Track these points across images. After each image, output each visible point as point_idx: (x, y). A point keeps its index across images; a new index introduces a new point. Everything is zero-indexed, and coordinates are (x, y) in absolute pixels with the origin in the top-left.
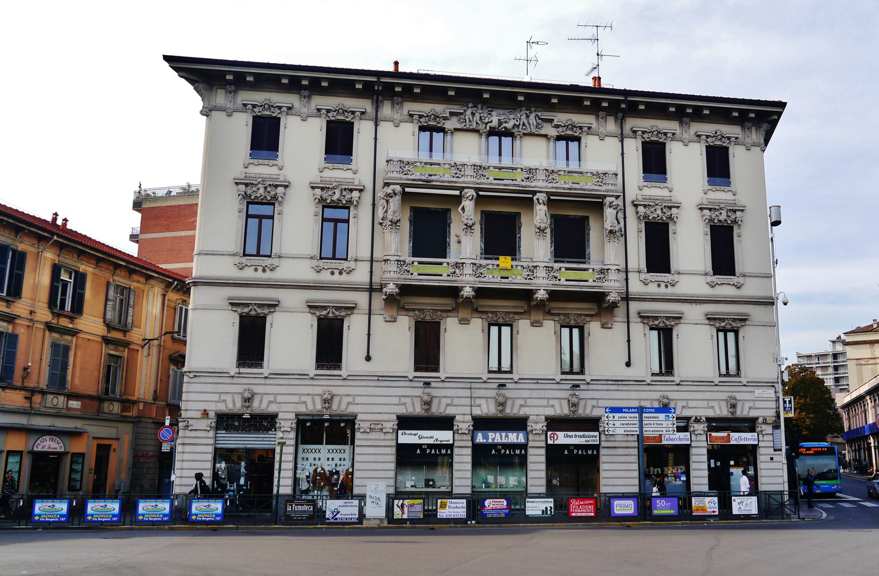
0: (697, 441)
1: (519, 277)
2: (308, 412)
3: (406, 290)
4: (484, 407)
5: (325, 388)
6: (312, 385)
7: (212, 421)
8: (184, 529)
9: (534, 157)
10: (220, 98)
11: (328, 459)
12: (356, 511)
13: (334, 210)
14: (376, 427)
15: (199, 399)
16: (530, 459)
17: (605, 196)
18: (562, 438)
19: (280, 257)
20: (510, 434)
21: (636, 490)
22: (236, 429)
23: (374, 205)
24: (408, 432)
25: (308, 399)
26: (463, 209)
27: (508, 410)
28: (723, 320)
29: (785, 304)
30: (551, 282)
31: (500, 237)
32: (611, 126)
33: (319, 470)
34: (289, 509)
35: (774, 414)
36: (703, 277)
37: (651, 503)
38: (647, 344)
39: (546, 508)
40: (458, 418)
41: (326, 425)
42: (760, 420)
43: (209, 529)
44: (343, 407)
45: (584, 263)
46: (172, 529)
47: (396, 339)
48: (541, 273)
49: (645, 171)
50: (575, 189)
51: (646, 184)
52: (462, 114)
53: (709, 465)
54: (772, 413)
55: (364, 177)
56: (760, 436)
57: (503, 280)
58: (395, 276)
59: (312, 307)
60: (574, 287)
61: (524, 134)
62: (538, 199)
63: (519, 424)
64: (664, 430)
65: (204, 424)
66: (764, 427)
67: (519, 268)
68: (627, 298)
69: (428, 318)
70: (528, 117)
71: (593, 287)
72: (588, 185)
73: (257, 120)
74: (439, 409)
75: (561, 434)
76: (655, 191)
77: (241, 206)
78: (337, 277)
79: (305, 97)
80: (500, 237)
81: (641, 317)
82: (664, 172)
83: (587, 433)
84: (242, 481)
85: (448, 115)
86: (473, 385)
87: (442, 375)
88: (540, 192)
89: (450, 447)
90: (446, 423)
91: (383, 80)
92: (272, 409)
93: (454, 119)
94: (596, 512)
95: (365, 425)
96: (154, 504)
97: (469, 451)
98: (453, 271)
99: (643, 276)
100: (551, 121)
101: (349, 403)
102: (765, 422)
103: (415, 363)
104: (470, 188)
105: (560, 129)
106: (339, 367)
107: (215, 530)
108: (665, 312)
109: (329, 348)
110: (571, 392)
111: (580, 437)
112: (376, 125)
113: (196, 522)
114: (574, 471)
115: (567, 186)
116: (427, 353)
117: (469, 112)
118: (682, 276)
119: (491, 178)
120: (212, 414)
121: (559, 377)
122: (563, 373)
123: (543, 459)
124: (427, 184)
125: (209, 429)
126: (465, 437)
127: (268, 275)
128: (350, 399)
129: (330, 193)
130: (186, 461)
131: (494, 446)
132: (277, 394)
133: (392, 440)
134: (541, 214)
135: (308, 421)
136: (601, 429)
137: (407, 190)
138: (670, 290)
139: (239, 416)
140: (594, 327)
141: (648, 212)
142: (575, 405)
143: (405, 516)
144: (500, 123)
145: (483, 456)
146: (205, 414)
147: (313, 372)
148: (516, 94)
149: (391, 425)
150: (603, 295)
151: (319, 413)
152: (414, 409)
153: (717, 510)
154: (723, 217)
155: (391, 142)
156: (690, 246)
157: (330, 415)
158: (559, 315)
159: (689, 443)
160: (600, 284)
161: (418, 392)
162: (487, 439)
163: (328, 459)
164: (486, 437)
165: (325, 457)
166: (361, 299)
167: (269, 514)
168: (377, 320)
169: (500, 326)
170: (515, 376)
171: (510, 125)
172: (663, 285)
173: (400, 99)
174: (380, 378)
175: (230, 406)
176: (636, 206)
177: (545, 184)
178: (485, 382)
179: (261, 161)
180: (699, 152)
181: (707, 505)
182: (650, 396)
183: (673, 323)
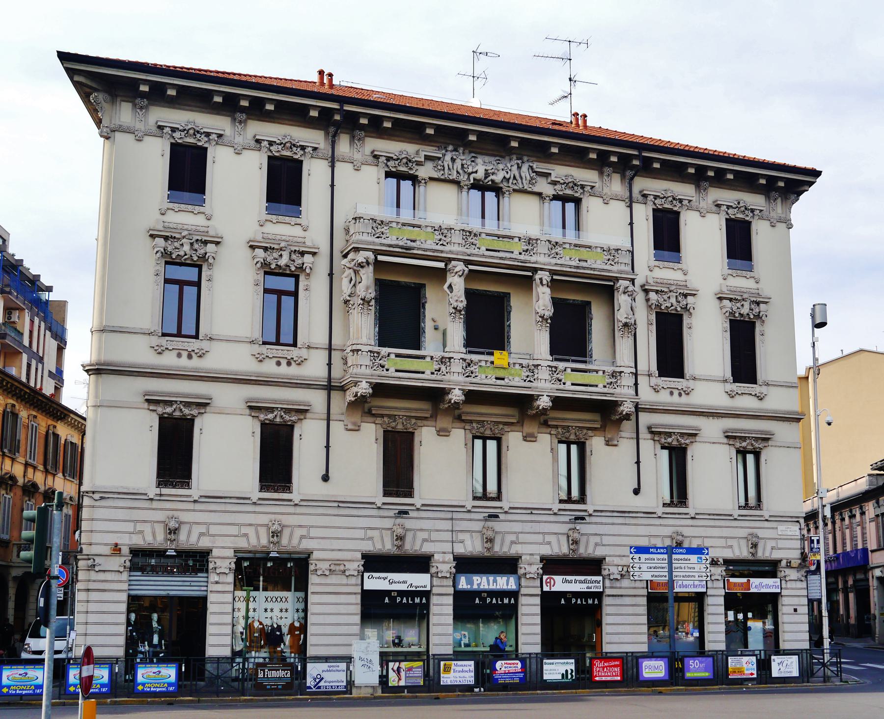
0: (713, 588)
1: (517, 379)
2: (250, 548)
3: (381, 390)
4: (377, 540)
5: (273, 517)
6: (255, 512)
7: (125, 559)
8: (131, 703)
9: (526, 220)
10: (125, 113)
11: (266, 610)
13: (281, 281)
14: (337, 568)
15: (106, 531)
16: (434, 609)
17: (617, 279)
18: (560, 584)
20: (499, 579)
22: (154, 570)
23: (331, 275)
24: (375, 575)
25: (251, 531)
26: (450, 287)
27: (497, 548)
28: (743, 439)
29: (829, 424)
30: (555, 386)
31: (486, 326)
32: (616, 185)
33: (256, 624)
34: (261, 675)
35: (799, 556)
36: (721, 385)
37: (683, 664)
38: (658, 464)
39: (567, 671)
40: (436, 557)
41: (269, 565)
42: (784, 563)
43: (431, 697)
44: (295, 542)
45: (585, 362)
46: (115, 703)
47: (360, 453)
48: (543, 374)
49: (269, 200)
50: (584, 268)
51: (657, 263)
52: (439, 158)
53: (128, 620)
54: (796, 554)
55: (317, 237)
56: (783, 582)
57: (499, 382)
58: (369, 371)
59: (254, 408)
61: (514, 190)
62: (541, 279)
64: (696, 574)
65: (116, 563)
68: (637, 408)
69: (400, 427)
70: (519, 168)
71: (605, 394)
73: (176, 149)
74: (414, 546)
75: (558, 579)
76: (667, 274)
77: (158, 267)
78: (284, 369)
79: (240, 122)
80: (486, 326)
81: (652, 432)
82: (202, 191)
83: (589, 578)
85: (423, 159)
86: (455, 516)
87: (417, 501)
88: (542, 269)
89: (426, 594)
90: (421, 563)
91: (347, 108)
92: (204, 543)
93: (429, 165)
94: (622, 675)
95: (324, 566)
96: (22, 671)
97: (450, 600)
98: (437, 367)
100: (547, 175)
102: (789, 565)
104: (459, 260)
105: (558, 187)
106: (188, 485)
107: (170, 704)
108: (679, 427)
109: (276, 463)
110: (572, 526)
111: (581, 582)
112: (333, 167)
113: (144, 694)
114: (572, 624)
116: (398, 474)
117: (448, 157)
118: (698, 383)
119: (483, 248)
120: (125, 550)
121: (556, 506)
122: (475, 498)
123: (538, 610)
124: (407, 252)
125: (122, 569)
127: (195, 363)
128: (303, 532)
130: (93, 612)
131: (478, 593)
132: (707, 537)
133: (643, 588)
134: (543, 299)
135: (246, 559)
136: (605, 573)
137: (380, 258)
138: (684, 399)
139: (160, 553)
141: (661, 301)
142: (401, 538)
143: (402, 683)
144: (487, 174)
145: (468, 608)
146: (116, 549)
148: (508, 138)
149: (356, 565)
150: (615, 404)
151: (264, 549)
152: (384, 546)
153: (755, 672)
154: (745, 310)
155: (350, 189)
156: (707, 345)
157: (176, 551)
158: (556, 427)
159: (704, 590)
160: (612, 391)
161: (388, 523)
162: (472, 584)
163: (266, 610)
165: (274, 608)
166: (316, 399)
167: (202, 683)
168: (337, 427)
169: (484, 439)
170: (505, 504)
171: (498, 178)
172: (676, 392)
173: (244, 116)
174: (341, 503)
175: (149, 538)
176: (646, 291)
177: (547, 260)
178: (469, 511)
179: (183, 207)
180: (718, 227)
181: (745, 666)
182: (659, 533)
183: (687, 441)
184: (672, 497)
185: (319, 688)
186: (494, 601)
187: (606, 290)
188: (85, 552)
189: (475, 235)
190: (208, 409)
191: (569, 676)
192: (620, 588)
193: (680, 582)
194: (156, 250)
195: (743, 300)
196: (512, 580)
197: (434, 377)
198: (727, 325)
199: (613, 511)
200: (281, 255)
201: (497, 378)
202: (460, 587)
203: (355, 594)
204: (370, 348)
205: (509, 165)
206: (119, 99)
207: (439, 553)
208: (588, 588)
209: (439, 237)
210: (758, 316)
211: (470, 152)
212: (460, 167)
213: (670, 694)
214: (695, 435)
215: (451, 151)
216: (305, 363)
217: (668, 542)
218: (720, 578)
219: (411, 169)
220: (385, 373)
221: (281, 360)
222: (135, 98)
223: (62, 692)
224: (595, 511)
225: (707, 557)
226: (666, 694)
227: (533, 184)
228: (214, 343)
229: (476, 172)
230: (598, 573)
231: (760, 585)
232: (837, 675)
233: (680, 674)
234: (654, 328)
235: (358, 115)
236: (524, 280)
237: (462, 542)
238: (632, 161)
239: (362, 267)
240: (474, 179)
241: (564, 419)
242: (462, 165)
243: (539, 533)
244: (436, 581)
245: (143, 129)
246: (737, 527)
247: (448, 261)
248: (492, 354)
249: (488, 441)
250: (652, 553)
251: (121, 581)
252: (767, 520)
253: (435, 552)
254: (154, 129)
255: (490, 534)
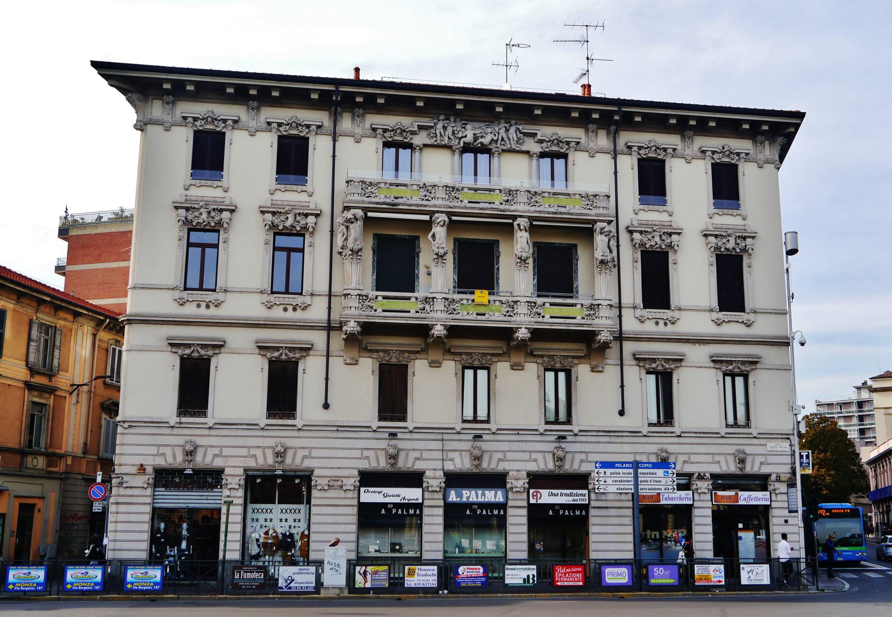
1: (497, 314)
2: (258, 467)
3: (369, 329)
5: (278, 440)
6: (263, 436)
7: (149, 477)
9: (515, 176)
10: (157, 110)
11: (281, 520)
12: (312, 578)
13: (287, 238)
14: (335, 484)
15: (133, 453)
17: (595, 221)
18: (546, 497)
19: (226, 291)
20: (487, 492)
21: (630, 555)
22: (177, 487)
24: (371, 489)
26: (434, 236)
27: (485, 465)
28: (730, 362)
29: (802, 344)
30: (534, 320)
31: (476, 267)
32: (602, 140)
34: (237, 577)
36: (707, 314)
37: (647, 571)
38: (643, 390)
39: (528, 576)
40: (428, 473)
42: (773, 477)
43: (393, 598)
45: (572, 297)
46: (104, 599)
47: (356, 385)
48: (522, 309)
50: (561, 213)
52: (432, 127)
54: (787, 469)
56: (773, 495)
57: (479, 317)
58: (357, 312)
59: (263, 348)
60: (560, 325)
62: (519, 225)
63: (498, 480)
66: (777, 485)
67: (497, 303)
68: (620, 337)
69: (394, 361)
70: (507, 130)
72: (576, 209)
74: (406, 463)
75: (545, 492)
76: (653, 215)
77: (181, 234)
80: (476, 267)
83: (575, 491)
84: (184, 545)
85: (416, 129)
86: (445, 437)
87: (410, 424)
88: (521, 216)
89: (419, 506)
90: (414, 479)
91: (342, 89)
92: (218, 463)
95: (323, 482)
96: (84, 571)
97: (441, 511)
98: (422, 306)
99: (639, 312)
100: (534, 135)
101: (304, 457)
102: (778, 480)
103: (379, 412)
105: (544, 145)
106: (204, 415)
107: (153, 600)
109: (282, 395)
111: (566, 495)
113: (132, 591)
114: (560, 535)
115: (552, 210)
116: (393, 400)
117: (440, 126)
118: (683, 313)
119: (466, 201)
120: (149, 470)
123: (525, 520)
124: (393, 208)
125: (146, 486)
126: (436, 496)
127: (213, 311)
129: (282, 218)
131: (469, 505)
132: (314, 448)
134: (522, 242)
135: (258, 476)
136: (591, 487)
137: (370, 214)
138: (670, 328)
139: (180, 472)
140: (582, 371)
141: (645, 240)
142: (561, 459)
143: (368, 585)
144: (476, 138)
145: (457, 518)
146: (142, 469)
147: (263, 421)
149: (352, 481)
151: (271, 468)
153: (723, 579)
154: (731, 245)
155: (351, 159)
156: (693, 278)
157: (283, 471)
160: (589, 322)
161: (383, 444)
162: (461, 497)
163: (281, 520)
164: (459, 495)
165: (278, 518)
166: (318, 338)
167: (214, 583)
168: (337, 363)
169: (475, 369)
171: (486, 140)
172: (661, 322)
173: (361, 111)
174: (340, 428)
175: (170, 460)
176: (631, 232)
177: (527, 208)
178: (459, 433)
181: (712, 573)
182: (647, 450)
183: (672, 366)
184: (659, 417)
185: (290, 588)
186: (567, 513)
187: (585, 231)
188: (116, 472)
189: (458, 190)
190: (223, 350)
191: (531, 581)
192: (606, 500)
193: (666, 495)
194: (709, 246)
195: (729, 235)
196: (499, 493)
197: (418, 315)
198: (714, 259)
199: (598, 431)
200: (287, 218)
201: (478, 314)
202: (450, 500)
203: (352, 506)
204: (528, 299)
205: (497, 129)
206: (151, 98)
207: (429, 470)
208: (573, 500)
209: (424, 193)
210: (745, 250)
211: (461, 120)
212: (451, 133)
213: (730, 601)
214: (681, 360)
215: (443, 120)
216: (309, 308)
217: (653, 459)
218: (706, 491)
219: (405, 138)
220: (541, 319)
221: (288, 307)
222: (588, 124)
223: (61, 589)
224: (580, 431)
225: (674, 471)
226: (628, 600)
227: (521, 144)
228: (228, 294)
229: (466, 136)
230: (585, 486)
231: (747, 498)
232: (813, 584)
233: (645, 581)
234: (639, 265)
235: (354, 95)
236: (505, 226)
237: (452, 460)
238: (708, 123)
239: (352, 223)
240: (464, 143)
241: (469, 347)
242: (453, 131)
243: (526, 451)
244: (427, 495)
245: (170, 120)
246: (724, 444)
247: (432, 213)
248: (473, 293)
249: (479, 371)
250: (617, 468)
251: (145, 496)
252: (755, 437)
253: (315, 468)
254: (180, 119)
255: (560, 453)
